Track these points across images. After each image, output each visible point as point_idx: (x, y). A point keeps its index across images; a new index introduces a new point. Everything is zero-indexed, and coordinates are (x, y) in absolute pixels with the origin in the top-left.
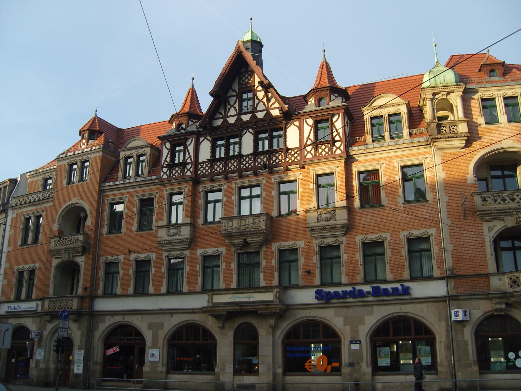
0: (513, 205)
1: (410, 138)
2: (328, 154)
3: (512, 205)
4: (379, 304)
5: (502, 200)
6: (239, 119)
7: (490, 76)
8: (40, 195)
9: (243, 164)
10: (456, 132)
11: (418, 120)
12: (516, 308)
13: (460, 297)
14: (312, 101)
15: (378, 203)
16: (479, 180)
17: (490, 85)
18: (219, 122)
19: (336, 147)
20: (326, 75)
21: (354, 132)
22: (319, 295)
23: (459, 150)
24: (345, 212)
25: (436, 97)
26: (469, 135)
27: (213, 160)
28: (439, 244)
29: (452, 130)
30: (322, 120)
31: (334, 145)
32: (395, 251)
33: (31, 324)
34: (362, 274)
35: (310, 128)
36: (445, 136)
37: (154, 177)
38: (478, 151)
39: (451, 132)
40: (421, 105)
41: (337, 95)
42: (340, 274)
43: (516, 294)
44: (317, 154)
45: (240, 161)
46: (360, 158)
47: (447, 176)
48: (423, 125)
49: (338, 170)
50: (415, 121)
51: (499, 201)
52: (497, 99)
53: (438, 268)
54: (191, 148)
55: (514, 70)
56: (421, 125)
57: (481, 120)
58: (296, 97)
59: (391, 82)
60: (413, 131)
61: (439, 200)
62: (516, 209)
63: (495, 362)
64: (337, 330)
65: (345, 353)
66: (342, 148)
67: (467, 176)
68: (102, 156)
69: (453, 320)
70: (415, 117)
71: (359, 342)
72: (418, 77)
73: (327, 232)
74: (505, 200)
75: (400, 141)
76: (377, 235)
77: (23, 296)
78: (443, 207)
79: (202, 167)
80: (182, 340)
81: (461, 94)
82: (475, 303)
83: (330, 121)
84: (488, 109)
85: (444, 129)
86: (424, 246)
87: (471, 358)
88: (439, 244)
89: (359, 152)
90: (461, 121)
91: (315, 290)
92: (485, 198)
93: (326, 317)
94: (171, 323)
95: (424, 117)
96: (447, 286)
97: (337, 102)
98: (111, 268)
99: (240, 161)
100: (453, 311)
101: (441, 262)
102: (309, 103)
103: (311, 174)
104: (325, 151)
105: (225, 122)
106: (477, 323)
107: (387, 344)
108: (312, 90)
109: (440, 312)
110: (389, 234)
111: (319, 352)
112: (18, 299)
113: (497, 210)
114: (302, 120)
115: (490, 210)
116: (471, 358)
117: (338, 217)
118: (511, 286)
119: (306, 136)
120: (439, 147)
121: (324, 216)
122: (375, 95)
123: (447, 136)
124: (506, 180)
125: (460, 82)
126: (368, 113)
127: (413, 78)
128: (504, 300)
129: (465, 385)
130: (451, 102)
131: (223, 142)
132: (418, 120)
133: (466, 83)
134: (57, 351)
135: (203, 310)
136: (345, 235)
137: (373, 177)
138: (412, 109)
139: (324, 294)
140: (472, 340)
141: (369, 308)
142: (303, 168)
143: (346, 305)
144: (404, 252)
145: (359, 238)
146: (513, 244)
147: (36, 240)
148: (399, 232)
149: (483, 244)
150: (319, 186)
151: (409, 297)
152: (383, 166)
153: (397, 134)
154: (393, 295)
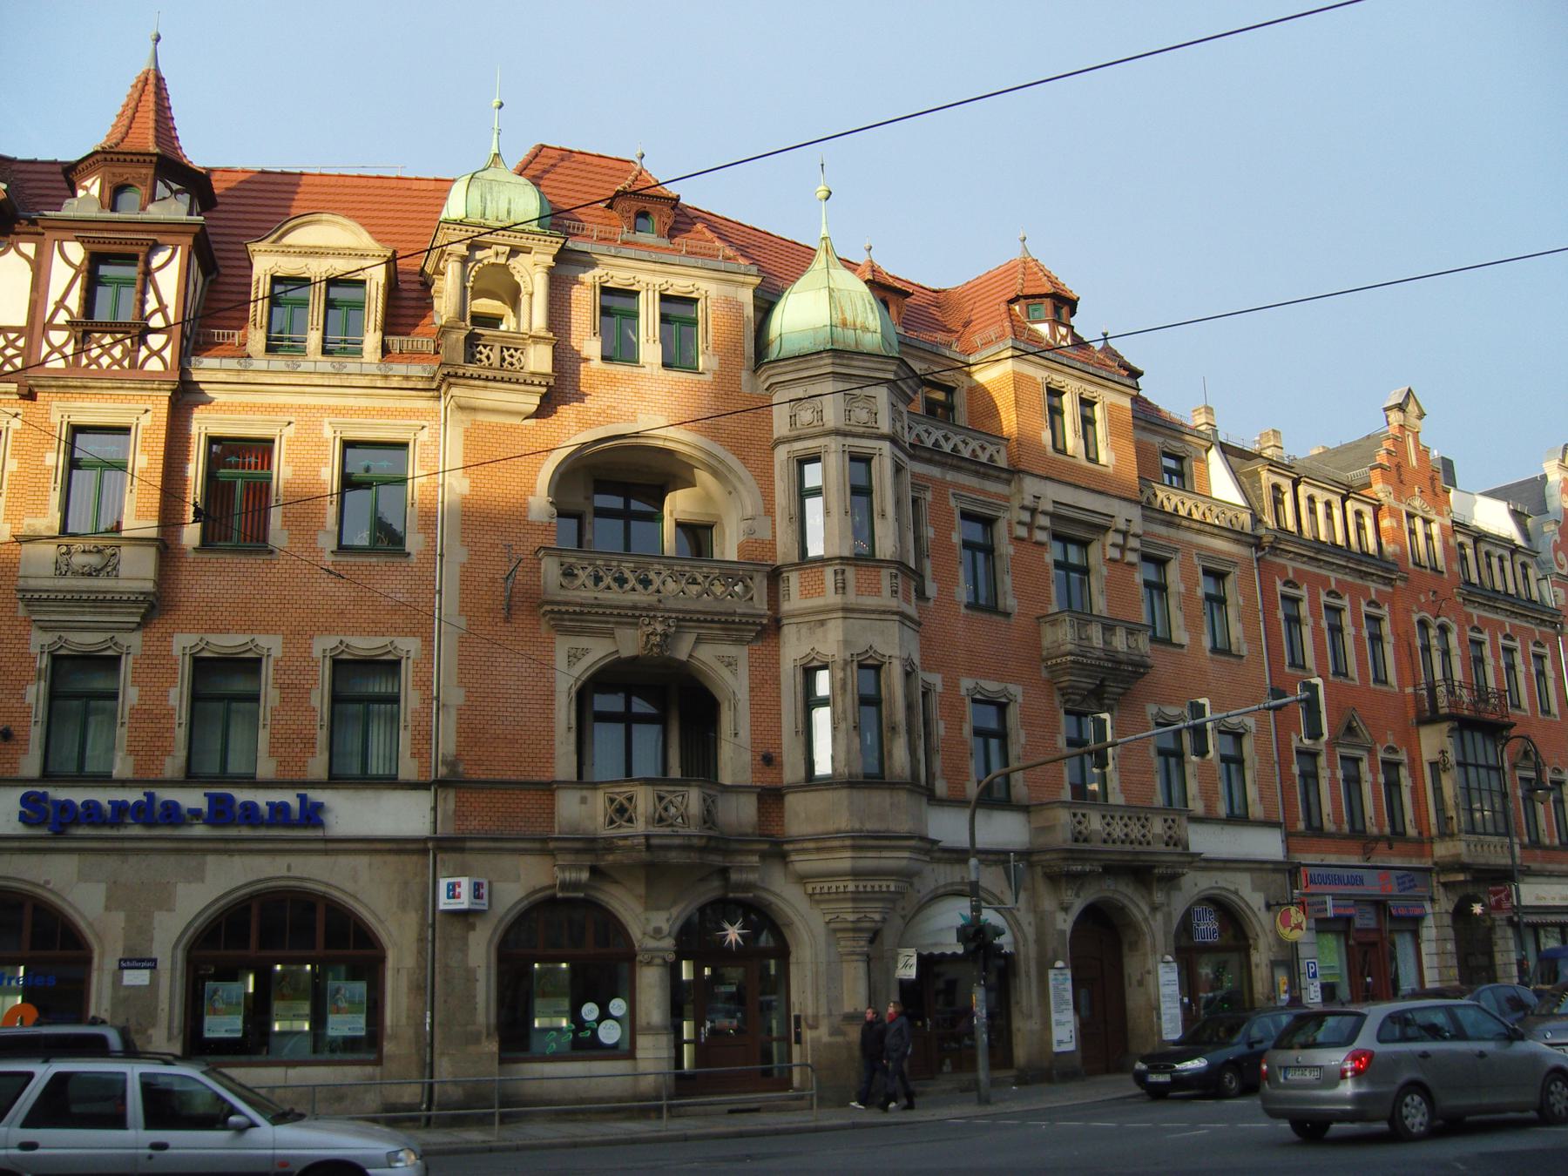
0: (644, 598)
1: (381, 361)
2: (121, 365)
3: (641, 597)
4: (226, 848)
5: (615, 580)
7: (636, 229)
9: (16, 348)
10: (518, 366)
11: (411, 312)
12: (616, 882)
13: (469, 845)
14: (92, 187)
15: (257, 542)
16: (561, 514)
17: (631, 253)
19: (149, 348)
20: (152, 115)
21: (214, 313)
22: (33, 809)
23: (517, 421)
24: (149, 556)
25: (479, 255)
26: (552, 383)
28: (424, 684)
29: (508, 359)
30: (113, 257)
31: (142, 340)
32: (293, 692)
33: (1250, 895)
34: (181, 754)
35: (73, 271)
36: (485, 373)
38: (573, 430)
39: (505, 364)
40: (429, 269)
41: (175, 186)
42: (111, 748)
43: (621, 843)
44: (84, 361)
46: (219, 396)
47: (473, 488)
48: (426, 330)
49: (146, 421)
50: (404, 312)
51: (608, 580)
52: (642, 297)
53: (413, 755)
55: (699, 226)
56: (418, 330)
57: (589, 346)
58: (34, 162)
59: (348, 182)
60: (395, 341)
61: (442, 555)
62: (650, 608)
63: (545, 1030)
64: (82, 925)
65: (99, 997)
66: (167, 354)
67: (531, 499)
69: (442, 906)
70: (407, 302)
71: (151, 964)
72: (432, 186)
73: (83, 613)
74: (626, 581)
75: (352, 365)
76: (378, 642)
78: (448, 579)
81: (549, 261)
82: (507, 862)
83: (141, 264)
84: (616, 320)
85: (486, 351)
86: (379, 687)
87: (481, 1018)
88: (424, 684)
89: (221, 376)
90: (537, 339)
91: (21, 791)
92: (571, 567)
93: (47, 882)
95: (430, 307)
96: (435, 809)
97: (174, 208)
100: (443, 884)
101: (424, 737)
102: (81, 193)
103: (55, 419)
104: (111, 356)
106: (509, 918)
107: (232, 974)
108: (96, 153)
109: (406, 883)
110: (280, 638)
111: (15, 993)
113: (599, 606)
114: (48, 243)
115: (581, 605)
116: (481, 1018)
117: (124, 570)
118: (612, 822)
120: (463, 402)
121: (78, 560)
122: (294, 212)
123: (490, 374)
124: (633, 523)
125: (554, 226)
126: (265, 263)
127: (416, 185)
128: (587, 860)
129: (456, 1093)
130: (517, 278)
132: (411, 312)
133: (568, 235)
136: (140, 626)
137: (253, 460)
138: (400, 277)
139: (50, 808)
140: (488, 968)
141: (190, 861)
142: (30, 396)
143: (118, 845)
144: (319, 699)
145: (183, 643)
146: (628, 704)
148: (311, 637)
149: (550, 696)
150: (73, 464)
151: (319, 833)
152: (289, 432)
153: (345, 341)
154: (270, 824)
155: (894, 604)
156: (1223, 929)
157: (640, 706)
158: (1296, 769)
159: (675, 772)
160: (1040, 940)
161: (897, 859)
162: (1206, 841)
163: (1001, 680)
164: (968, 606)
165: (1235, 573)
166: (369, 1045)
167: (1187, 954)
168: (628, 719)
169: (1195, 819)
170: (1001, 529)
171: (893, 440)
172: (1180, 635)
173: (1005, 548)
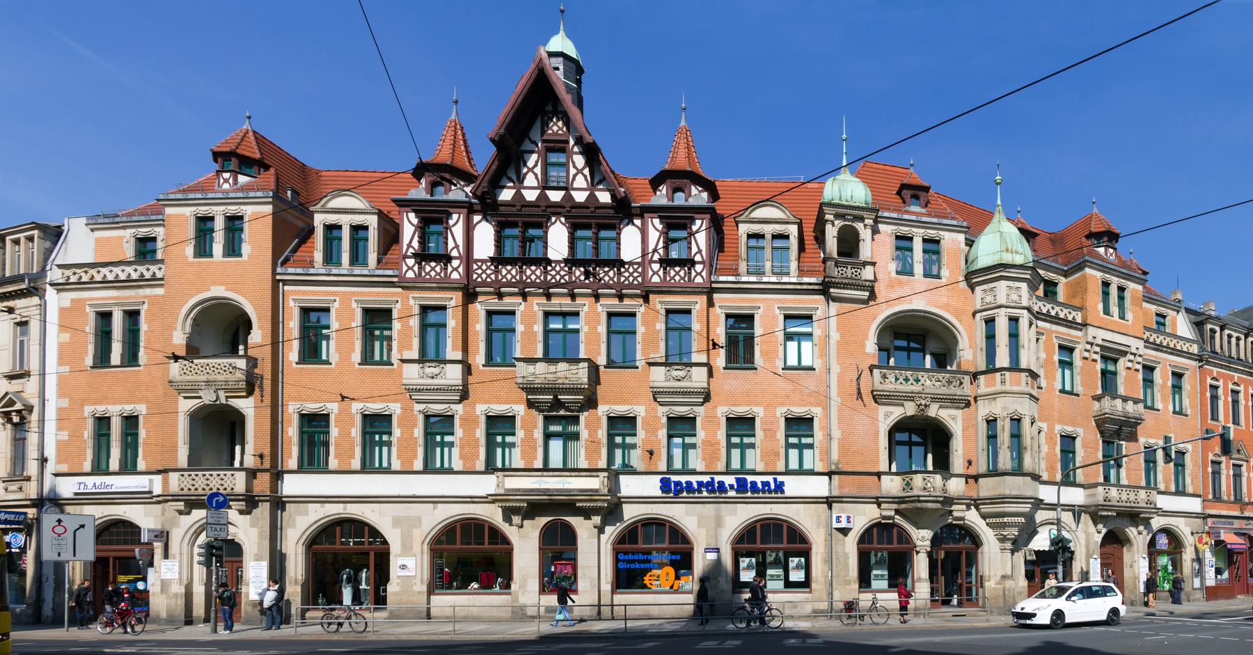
3: (916, 388)
6: (543, 197)
8: (129, 269)
18: (506, 195)
22: (665, 485)
27: (499, 260)
33: (1183, 527)
37: (390, 272)
45: (545, 268)
51: (901, 380)
54: (458, 231)
68: (274, 214)
77: (114, 464)
79: (480, 268)
80: (455, 543)
94: (435, 518)
98: (314, 425)
99: (545, 268)
101: (827, 452)
105: (519, 196)
112: (99, 468)
119: (651, 247)
128: (895, 506)
131: (588, 233)
134: (208, 564)
135: (491, 499)
145: (481, 409)
147: (131, 357)
149: (877, 433)
155: (1028, 389)
156: (1170, 543)
157: (915, 438)
158: (1210, 470)
159: (930, 468)
160: (1087, 547)
161: (1026, 508)
162: (1164, 502)
163: (1073, 425)
164: (1061, 391)
165: (1187, 374)
166: (806, 584)
167: (1153, 551)
168: (910, 444)
169: (1160, 493)
170: (1077, 354)
171: (1029, 309)
172: (1159, 405)
173: (1078, 362)
